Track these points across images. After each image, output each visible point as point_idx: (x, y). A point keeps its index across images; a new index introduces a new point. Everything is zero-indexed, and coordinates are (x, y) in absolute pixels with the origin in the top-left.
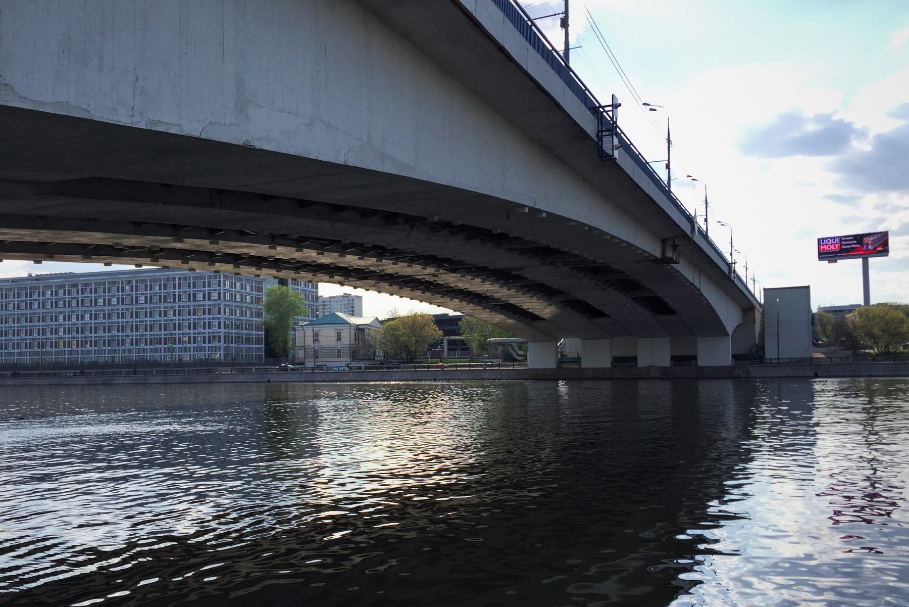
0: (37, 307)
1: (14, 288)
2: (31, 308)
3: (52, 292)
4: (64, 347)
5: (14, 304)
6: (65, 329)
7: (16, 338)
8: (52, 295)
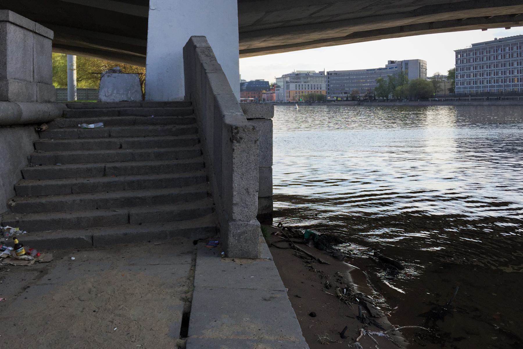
0: (500, 58)
1: (518, 43)
2: (497, 59)
3: (509, 48)
4: (518, 82)
5: (487, 57)
6: (518, 71)
7: (488, 77)
8: (509, 50)
